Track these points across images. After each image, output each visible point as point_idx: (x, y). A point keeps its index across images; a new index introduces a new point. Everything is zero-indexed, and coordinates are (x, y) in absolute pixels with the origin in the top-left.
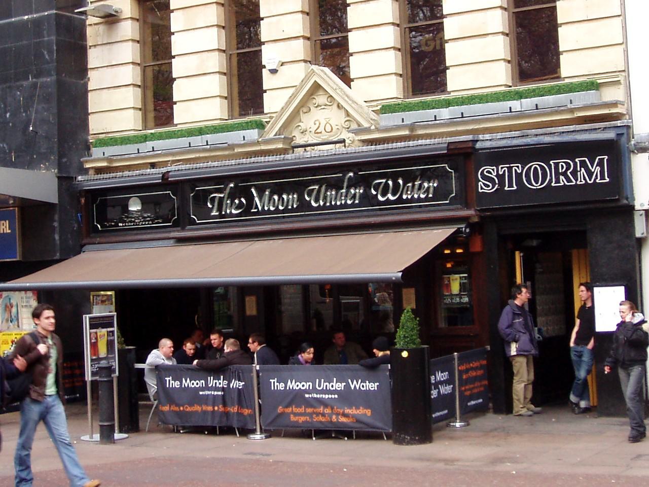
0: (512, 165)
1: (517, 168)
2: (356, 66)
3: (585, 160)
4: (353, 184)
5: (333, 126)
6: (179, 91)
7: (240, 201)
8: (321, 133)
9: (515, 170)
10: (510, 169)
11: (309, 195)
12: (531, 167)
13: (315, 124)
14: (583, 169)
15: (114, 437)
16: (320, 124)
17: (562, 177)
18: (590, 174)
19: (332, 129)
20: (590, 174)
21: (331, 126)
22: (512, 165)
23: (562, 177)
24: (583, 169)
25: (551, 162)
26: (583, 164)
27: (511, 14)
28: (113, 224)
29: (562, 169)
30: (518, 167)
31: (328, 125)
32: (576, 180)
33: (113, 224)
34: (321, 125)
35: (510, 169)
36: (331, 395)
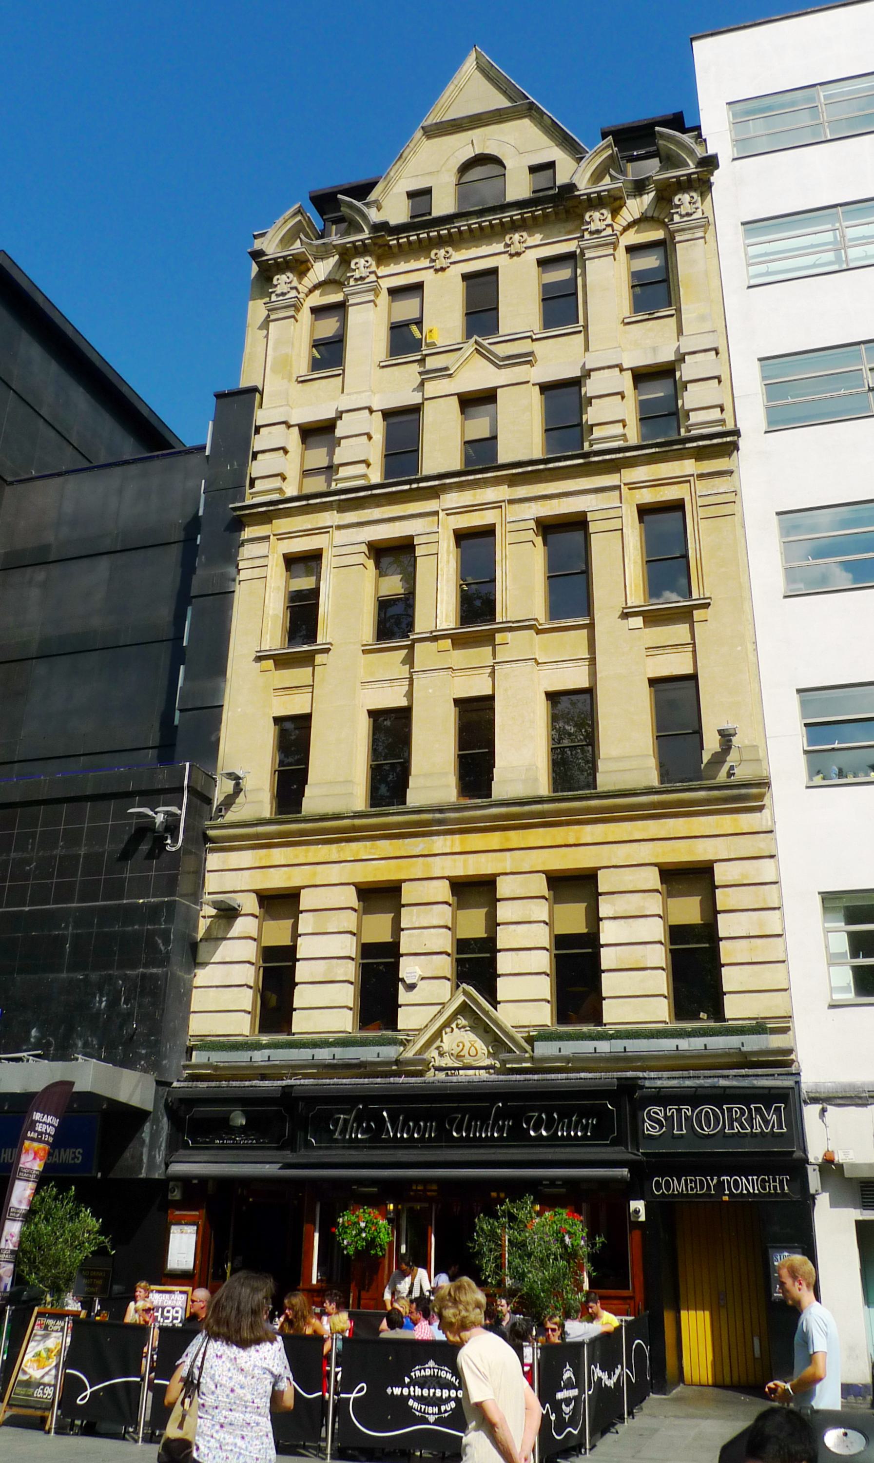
0: (681, 1107)
1: (686, 1110)
2: (504, 988)
3: (761, 1107)
4: (500, 1115)
5: (478, 1049)
6: (301, 997)
7: (369, 1125)
8: (464, 1056)
9: (685, 1112)
10: (679, 1111)
11: (528, 1124)
12: (703, 1109)
13: (458, 1046)
14: (758, 1116)
15: (860, 1453)
16: (464, 1046)
17: (736, 1124)
18: (766, 1122)
19: (477, 1053)
20: (766, 1122)
21: (476, 1049)
22: (681, 1107)
23: (736, 1124)
24: (774, 1116)
25: (724, 1107)
26: (758, 1110)
27: (553, 956)
28: (207, 1140)
29: (736, 1115)
30: (688, 1109)
31: (473, 1048)
32: (752, 1128)
33: (207, 1140)
34: (465, 1048)
35: (679, 1111)
36: (426, 1377)
